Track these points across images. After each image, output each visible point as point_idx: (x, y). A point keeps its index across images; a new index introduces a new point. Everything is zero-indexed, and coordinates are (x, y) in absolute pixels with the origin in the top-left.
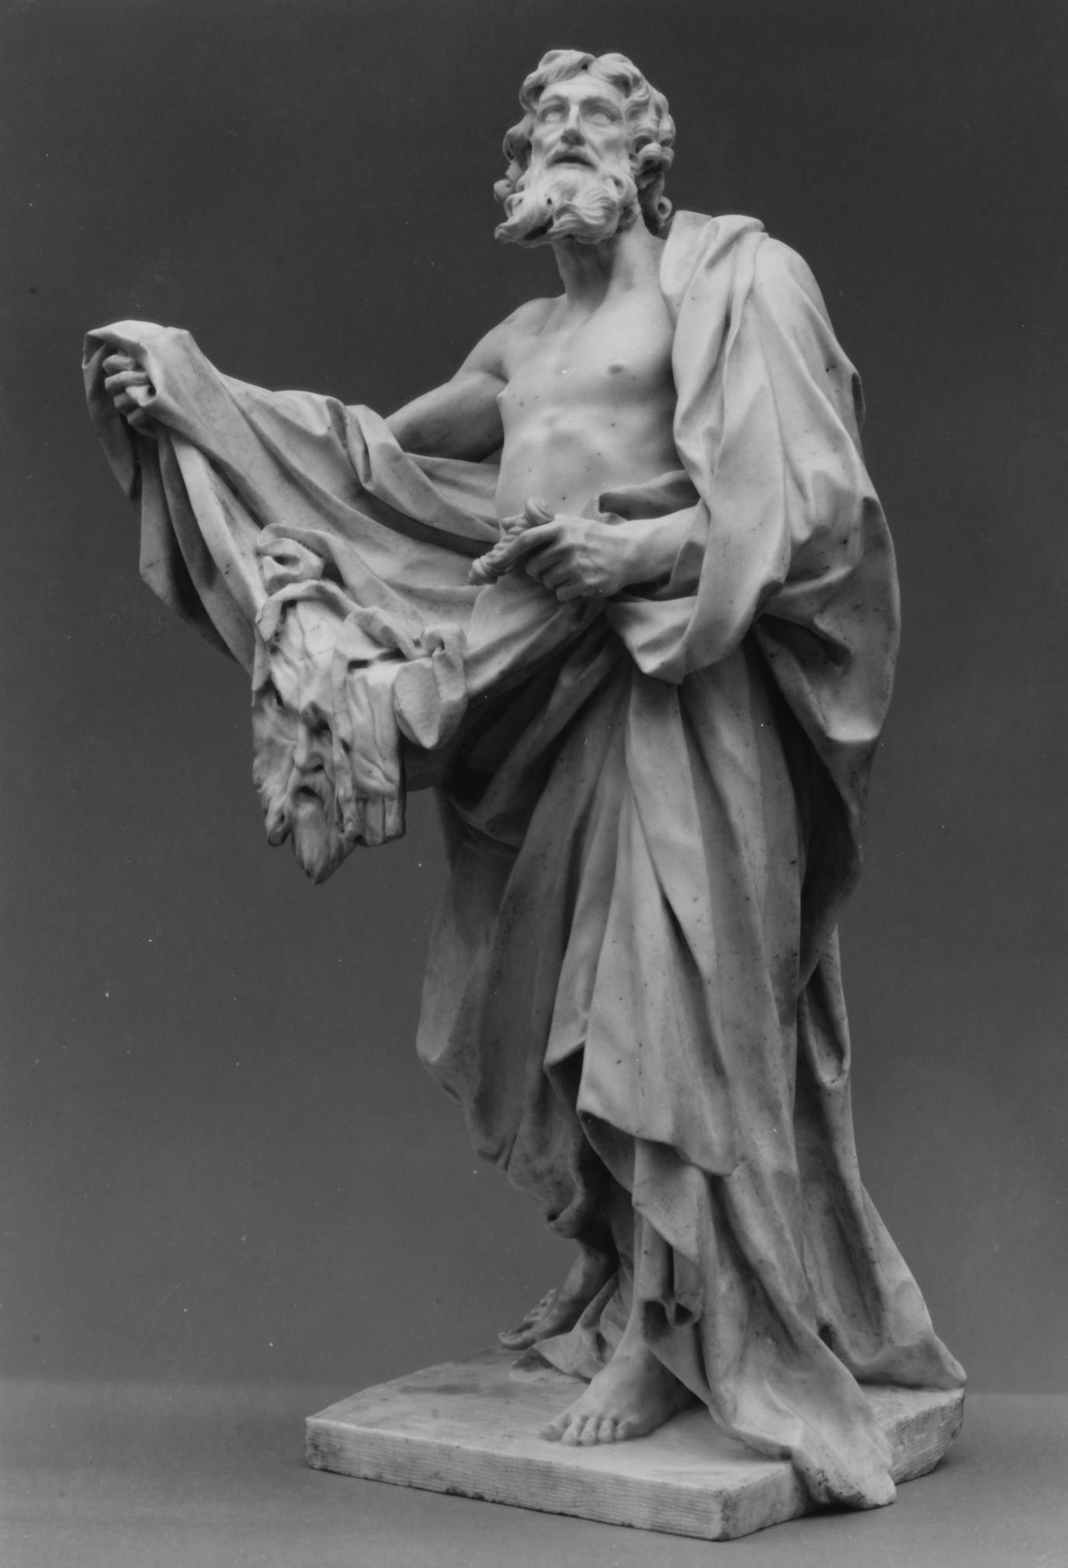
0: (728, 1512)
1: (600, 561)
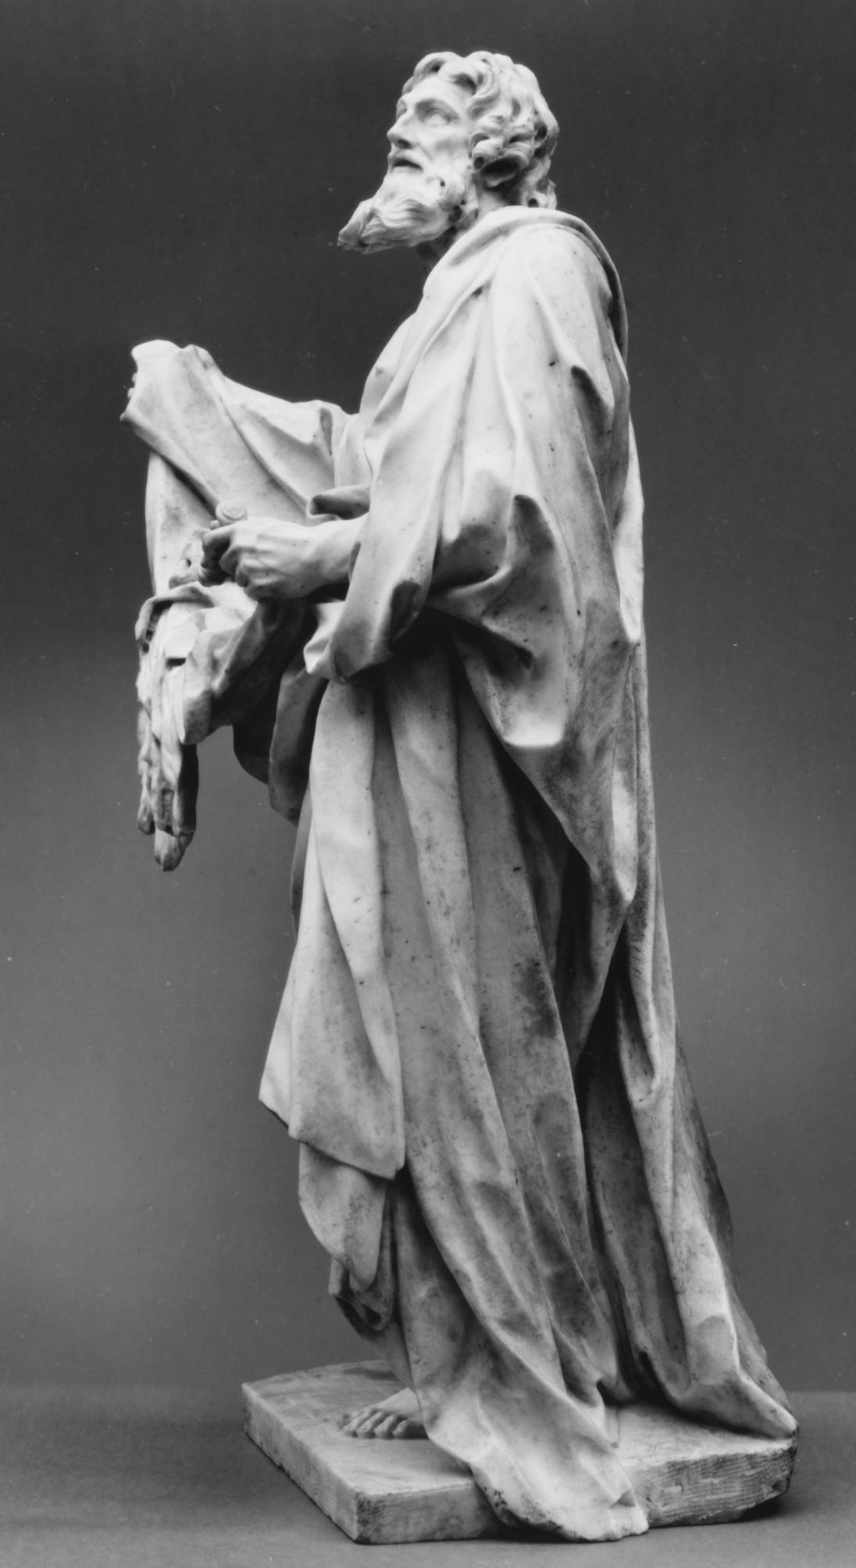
0: (364, 1516)
1: (271, 562)
